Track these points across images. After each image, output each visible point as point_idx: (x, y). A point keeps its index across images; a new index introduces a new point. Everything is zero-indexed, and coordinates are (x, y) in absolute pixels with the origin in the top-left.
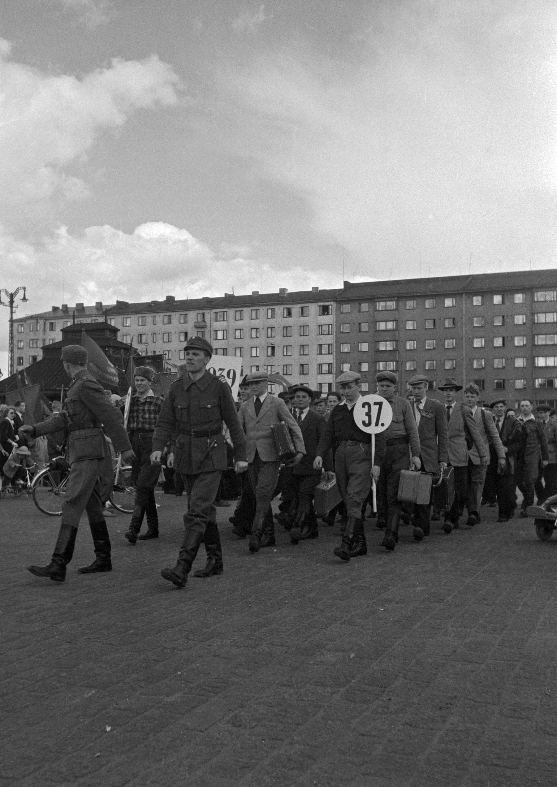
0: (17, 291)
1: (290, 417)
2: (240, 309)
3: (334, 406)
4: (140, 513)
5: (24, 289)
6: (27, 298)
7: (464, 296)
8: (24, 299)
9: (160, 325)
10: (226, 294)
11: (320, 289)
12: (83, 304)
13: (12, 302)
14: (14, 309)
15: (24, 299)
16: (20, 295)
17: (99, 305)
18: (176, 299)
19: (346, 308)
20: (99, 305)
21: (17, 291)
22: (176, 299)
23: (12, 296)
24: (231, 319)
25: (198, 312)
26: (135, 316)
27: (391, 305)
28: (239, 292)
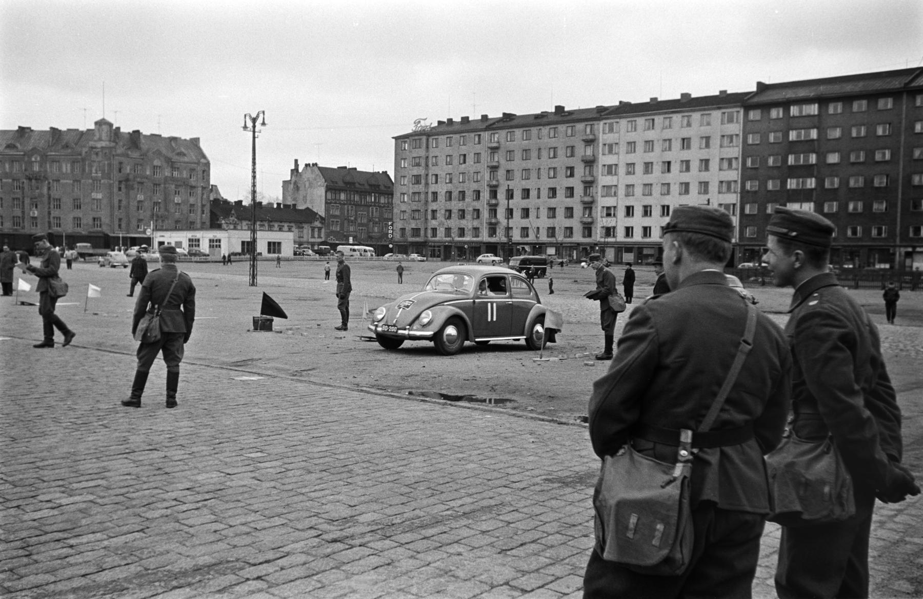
0: (258, 116)
1: (60, 498)
2: (554, 126)
3: (649, 326)
4: (834, 465)
5: (264, 112)
6: (266, 122)
7: (905, 96)
8: (264, 124)
9: (546, 140)
10: (621, 102)
11: (729, 92)
12: (468, 118)
13: (254, 127)
14: (256, 134)
15: (264, 124)
16: (260, 121)
17: (485, 117)
18: (566, 109)
19: (754, 115)
20: (485, 117)
21: (258, 116)
22: (566, 109)
23: (254, 121)
24: (623, 131)
25: (586, 123)
26: (562, 125)
27: (814, 109)
28: (662, 98)
